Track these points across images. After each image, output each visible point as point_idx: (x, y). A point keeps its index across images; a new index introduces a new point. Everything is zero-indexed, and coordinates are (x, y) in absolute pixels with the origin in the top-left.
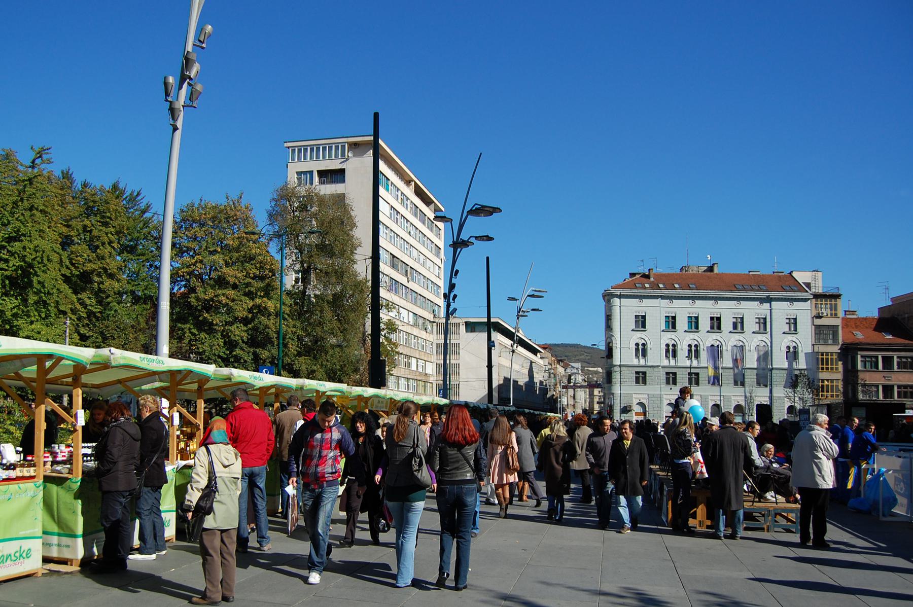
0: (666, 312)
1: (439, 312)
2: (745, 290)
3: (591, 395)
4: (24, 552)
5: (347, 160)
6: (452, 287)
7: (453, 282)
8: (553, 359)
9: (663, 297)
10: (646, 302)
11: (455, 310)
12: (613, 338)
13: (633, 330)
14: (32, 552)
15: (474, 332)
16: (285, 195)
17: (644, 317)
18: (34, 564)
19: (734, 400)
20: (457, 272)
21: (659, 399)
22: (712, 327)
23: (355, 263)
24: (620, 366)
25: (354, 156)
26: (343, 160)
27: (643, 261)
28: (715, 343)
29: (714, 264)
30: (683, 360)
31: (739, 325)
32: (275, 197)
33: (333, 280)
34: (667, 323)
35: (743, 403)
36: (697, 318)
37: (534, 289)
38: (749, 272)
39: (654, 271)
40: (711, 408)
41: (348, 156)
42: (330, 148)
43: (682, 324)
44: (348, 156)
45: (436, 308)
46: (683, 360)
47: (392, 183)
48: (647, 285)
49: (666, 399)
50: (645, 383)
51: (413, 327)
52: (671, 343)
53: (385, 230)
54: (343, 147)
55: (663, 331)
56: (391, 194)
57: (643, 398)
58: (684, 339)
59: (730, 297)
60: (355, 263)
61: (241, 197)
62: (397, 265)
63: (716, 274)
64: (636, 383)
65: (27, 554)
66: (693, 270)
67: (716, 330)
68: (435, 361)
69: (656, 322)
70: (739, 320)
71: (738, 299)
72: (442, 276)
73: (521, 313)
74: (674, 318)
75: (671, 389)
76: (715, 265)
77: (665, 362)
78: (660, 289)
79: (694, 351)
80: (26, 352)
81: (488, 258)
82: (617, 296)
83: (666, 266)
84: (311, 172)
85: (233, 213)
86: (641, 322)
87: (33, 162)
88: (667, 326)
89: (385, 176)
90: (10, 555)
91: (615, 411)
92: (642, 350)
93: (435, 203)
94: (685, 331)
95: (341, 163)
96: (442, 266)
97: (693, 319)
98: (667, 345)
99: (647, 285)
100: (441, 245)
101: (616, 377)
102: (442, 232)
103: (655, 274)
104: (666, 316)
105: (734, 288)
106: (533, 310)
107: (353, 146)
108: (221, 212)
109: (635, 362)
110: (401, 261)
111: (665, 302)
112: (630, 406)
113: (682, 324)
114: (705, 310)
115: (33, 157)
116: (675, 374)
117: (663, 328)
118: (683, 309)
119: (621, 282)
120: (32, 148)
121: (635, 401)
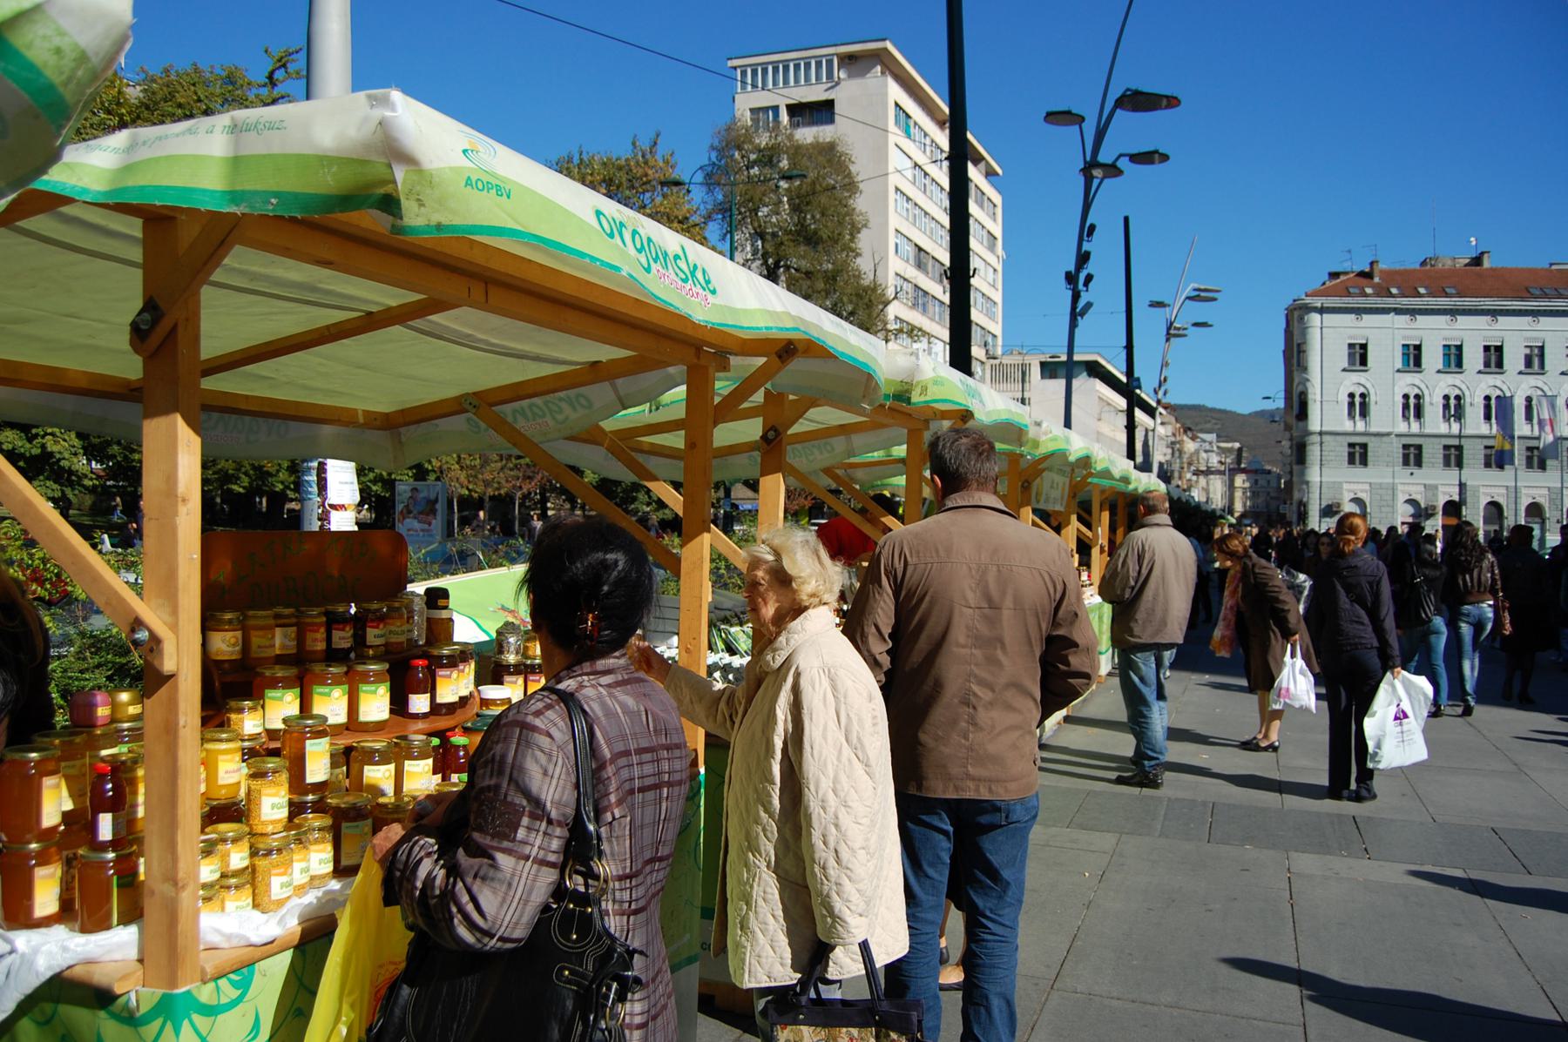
0: (1404, 338)
1: (995, 346)
2: (1546, 296)
3: (1231, 487)
5: (837, 84)
6: (1083, 258)
7: (1084, 249)
8: (1178, 425)
9: (1398, 311)
10: (1368, 319)
11: (1089, 305)
12: (1308, 384)
13: (1344, 370)
16: (732, 140)
17: (1364, 347)
19: (1527, 495)
20: (1092, 228)
21: (1390, 492)
22: (1487, 364)
23: (858, 255)
24: (1321, 433)
25: (850, 76)
26: (830, 85)
27: (1349, 251)
28: (1493, 392)
29: (1482, 253)
30: (1434, 421)
31: (1536, 361)
32: (716, 143)
33: (820, 285)
34: (1406, 357)
35: (1502, 501)
36: (1459, 348)
37: (1196, 286)
38: (1551, 265)
39: (1382, 266)
40: (1485, 508)
41: (839, 78)
42: (808, 66)
43: (1433, 358)
44: (839, 78)
45: (990, 340)
46: (1434, 421)
47: (916, 124)
48: (1369, 291)
49: (1403, 492)
50: (1364, 462)
52: (1413, 392)
53: (905, 205)
54: (830, 63)
55: (1398, 371)
57: (1362, 491)
58: (1435, 385)
59: (1520, 310)
60: (858, 255)
61: (655, 143)
62: (926, 265)
63: (1487, 269)
64: (1528, 468)
66: (1445, 263)
67: (1493, 369)
69: (1386, 355)
70: (1536, 351)
71: (1535, 313)
72: (1000, 285)
73: (1172, 332)
74: (1418, 348)
75: (1412, 474)
76: (1486, 255)
77: (1402, 427)
78: (1392, 296)
79: (1454, 408)
81: (1126, 220)
82: (1315, 310)
83: (1399, 256)
84: (776, 109)
85: (640, 172)
86: (1359, 355)
87: (271, 76)
88: (1406, 362)
89: (904, 111)
91: (1311, 513)
92: (1360, 405)
93: (987, 163)
94: (1439, 372)
95: (826, 90)
96: (1000, 268)
97: (1453, 350)
98: (1406, 397)
99: (1369, 291)
100: (998, 232)
101: (1313, 453)
102: (999, 211)
103: (1381, 271)
104: (1403, 345)
105: (1526, 294)
106: (1196, 325)
107: (847, 61)
108: (620, 168)
109: (1348, 426)
110: (933, 258)
111: (1403, 320)
112: (1339, 505)
113: (1433, 358)
114: (1473, 332)
115: (270, 68)
116: (1419, 447)
117: (1399, 365)
118: (1434, 332)
119: (1317, 286)
120: (266, 51)
121: (1347, 496)
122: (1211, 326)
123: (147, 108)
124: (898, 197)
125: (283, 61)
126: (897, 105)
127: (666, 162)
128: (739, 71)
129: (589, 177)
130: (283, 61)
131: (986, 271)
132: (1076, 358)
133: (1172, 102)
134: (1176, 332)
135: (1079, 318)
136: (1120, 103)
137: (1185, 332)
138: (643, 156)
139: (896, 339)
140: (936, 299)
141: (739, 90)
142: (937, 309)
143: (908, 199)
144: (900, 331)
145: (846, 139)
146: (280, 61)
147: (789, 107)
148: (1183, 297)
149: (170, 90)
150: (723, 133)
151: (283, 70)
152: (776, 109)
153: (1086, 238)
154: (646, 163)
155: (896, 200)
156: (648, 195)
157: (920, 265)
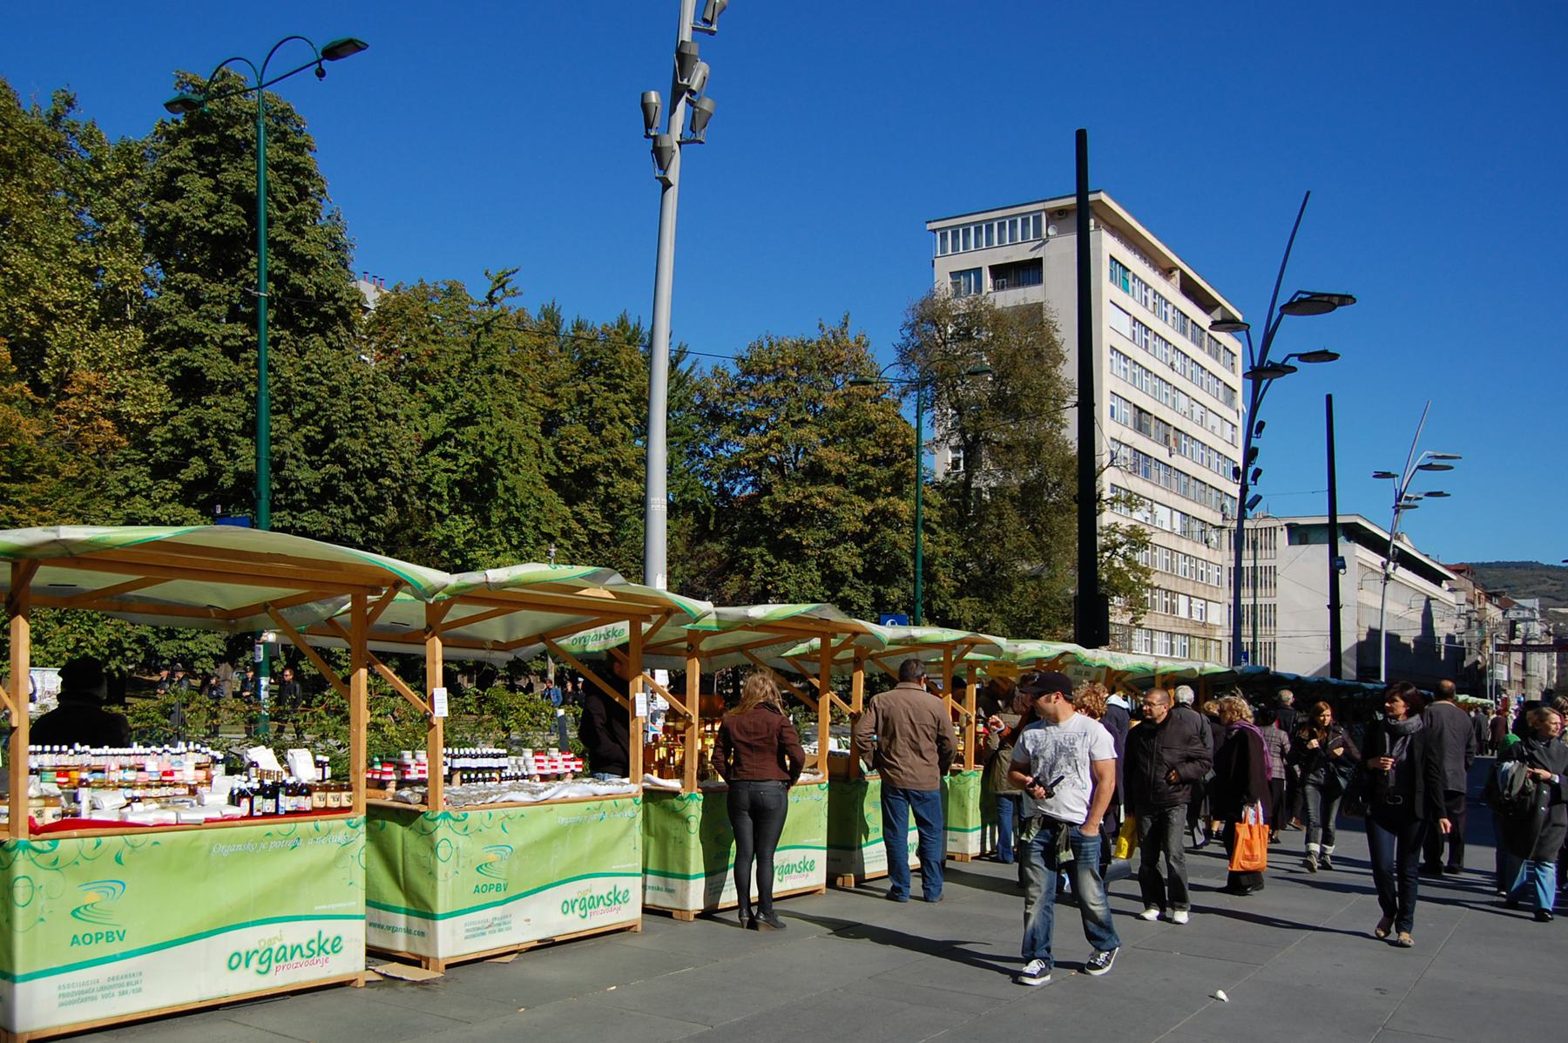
4: (327, 940)
5: (1045, 242)
8: (1477, 591)
16: (929, 315)
20: (1261, 425)
26: (1038, 243)
37: (1431, 453)
41: (1048, 235)
44: (1048, 235)
47: (1135, 276)
53: (1123, 364)
54: (1037, 220)
60: (1066, 426)
62: (1147, 426)
65: (333, 947)
80: (252, 584)
84: (978, 271)
87: (490, 296)
89: (1121, 265)
93: (1224, 307)
106: (1429, 494)
107: (1057, 216)
110: (1156, 418)
120: (486, 274)
122: (1448, 495)
123: (380, 323)
124: (1114, 358)
125: (502, 281)
126: (1112, 258)
127: (858, 342)
128: (938, 234)
129: (781, 362)
130: (502, 281)
131: (1222, 429)
132: (1340, 520)
133: (1346, 299)
134: (1407, 503)
135: (1248, 510)
136: (1286, 308)
137: (1416, 503)
138: (834, 337)
139: (1112, 508)
140: (1160, 462)
141: (939, 255)
142: (1162, 473)
143: (1126, 358)
144: (1116, 500)
145: (1050, 305)
146: (498, 281)
147: (992, 268)
148: (1415, 466)
149: (401, 306)
150: (918, 307)
151: (501, 290)
152: (978, 271)
153: (1254, 434)
154: (837, 343)
155: (1111, 360)
156: (840, 376)
157: (1140, 428)
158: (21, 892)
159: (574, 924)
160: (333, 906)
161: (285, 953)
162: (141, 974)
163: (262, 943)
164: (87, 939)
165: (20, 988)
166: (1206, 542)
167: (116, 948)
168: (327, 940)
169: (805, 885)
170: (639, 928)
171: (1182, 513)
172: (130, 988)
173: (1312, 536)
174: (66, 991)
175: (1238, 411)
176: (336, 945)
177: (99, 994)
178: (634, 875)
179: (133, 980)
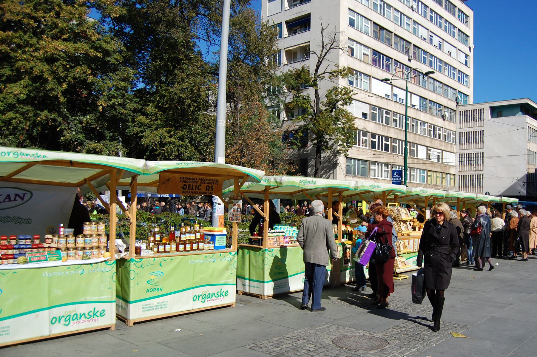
4: (98, 312)
14: (228, 293)
15: (501, 116)
18: (231, 299)
51: (419, 112)
56: (451, 12)
65: (225, 294)
68: (458, 151)
80: (88, 162)
90: (214, 294)
96: (471, 55)
158: (132, 275)
159: (59, 329)
160: (102, 297)
161: (77, 317)
162: (9, 327)
163: (66, 313)
164: (151, 290)
165: (132, 306)
166: (443, 117)
167: (160, 293)
168: (98, 312)
169: (155, 314)
170: (234, 306)
171: (420, 97)
172: (4, 333)
173: (504, 113)
174: (144, 307)
175: (470, 48)
176: (226, 293)
177: (155, 308)
178: (111, 302)
179: (6, 329)
